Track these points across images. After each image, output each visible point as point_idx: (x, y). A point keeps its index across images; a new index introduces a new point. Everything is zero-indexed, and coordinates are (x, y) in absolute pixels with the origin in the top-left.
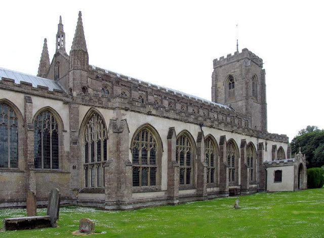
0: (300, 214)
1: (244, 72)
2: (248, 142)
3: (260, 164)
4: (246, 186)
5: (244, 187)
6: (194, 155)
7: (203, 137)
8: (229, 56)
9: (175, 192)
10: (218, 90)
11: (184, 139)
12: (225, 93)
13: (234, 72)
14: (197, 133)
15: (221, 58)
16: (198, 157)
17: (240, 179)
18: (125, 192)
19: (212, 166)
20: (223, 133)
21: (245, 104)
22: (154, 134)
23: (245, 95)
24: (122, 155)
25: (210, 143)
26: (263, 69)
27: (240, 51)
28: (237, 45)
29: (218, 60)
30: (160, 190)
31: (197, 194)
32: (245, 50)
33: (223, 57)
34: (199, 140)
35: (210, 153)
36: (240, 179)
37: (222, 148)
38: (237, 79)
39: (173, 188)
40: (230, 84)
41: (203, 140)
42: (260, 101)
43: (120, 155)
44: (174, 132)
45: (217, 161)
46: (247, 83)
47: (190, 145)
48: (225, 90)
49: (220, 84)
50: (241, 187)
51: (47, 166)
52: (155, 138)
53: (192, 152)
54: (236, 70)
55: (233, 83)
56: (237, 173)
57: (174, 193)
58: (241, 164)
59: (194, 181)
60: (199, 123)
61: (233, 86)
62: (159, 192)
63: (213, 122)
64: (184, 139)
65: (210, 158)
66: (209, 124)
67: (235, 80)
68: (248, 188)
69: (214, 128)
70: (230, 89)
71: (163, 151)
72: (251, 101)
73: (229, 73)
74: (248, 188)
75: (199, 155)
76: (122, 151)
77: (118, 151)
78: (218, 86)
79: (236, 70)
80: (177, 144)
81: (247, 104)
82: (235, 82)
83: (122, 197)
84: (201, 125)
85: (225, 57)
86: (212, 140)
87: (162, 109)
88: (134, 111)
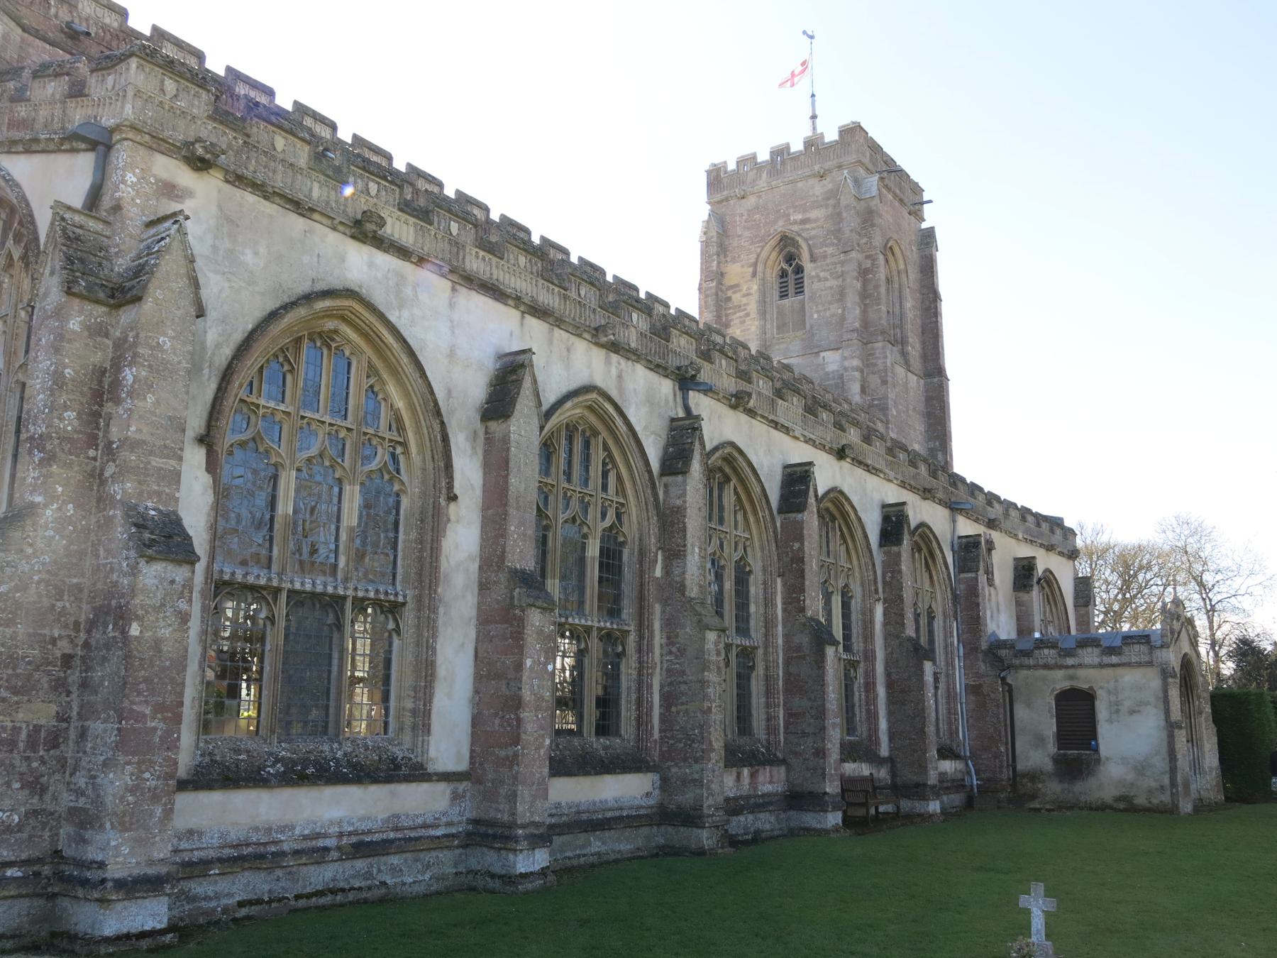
0: (582, 561)
1: (851, 222)
2: (914, 519)
3: (971, 649)
4: (923, 768)
5: (909, 776)
6: (642, 553)
7: (697, 447)
8: (781, 153)
9: (524, 793)
10: (729, 299)
11: (587, 445)
12: (763, 313)
13: (804, 222)
14: (661, 426)
15: (741, 162)
16: (667, 570)
17: (883, 725)
18: (115, 784)
19: (743, 630)
20: (799, 453)
21: (856, 363)
22: (395, 372)
23: (857, 325)
24: (117, 477)
25: (729, 499)
26: (924, 225)
27: (831, 135)
28: (814, 117)
29: (732, 166)
30: (417, 773)
31: (661, 805)
32: (853, 132)
33: (754, 157)
34: (676, 460)
35: (730, 557)
36: (883, 725)
37: (796, 533)
38: (818, 251)
39: (513, 760)
40: (783, 274)
41: (696, 466)
42: (916, 363)
43: (110, 470)
44: (527, 383)
45: (768, 602)
46: (864, 273)
47: (621, 490)
48: (763, 302)
49: (736, 272)
50: (893, 774)
51: (374, 562)
52: (400, 404)
53: (630, 529)
54: (813, 214)
55: (799, 270)
56: (870, 686)
57: (512, 798)
58: (887, 636)
59: (642, 721)
60: (673, 362)
61: (800, 289)
62: (403, 788)
63: (743, 376)
64: (587, 445)
65: (728, 585)
66: (729, 384)
67: (805, 255)
68: (932, 779)
69: (751, 413)
70: (783, 295)
71: (454, 498)
72: (888, 356)
73: (780, 226)
74: (932, 779)
75: (675, 554)
76: (124, 442)
77: (92, 441)
78: (730, 280)
79: (813, 214)
80: (546, 471)
81: (868, 362)
82: (808, 266)
83: (85, 820)
84: (686, 381)
85: (763, 156)
86: (742, 480)
87: (454, 227)
88: (259, 188)
